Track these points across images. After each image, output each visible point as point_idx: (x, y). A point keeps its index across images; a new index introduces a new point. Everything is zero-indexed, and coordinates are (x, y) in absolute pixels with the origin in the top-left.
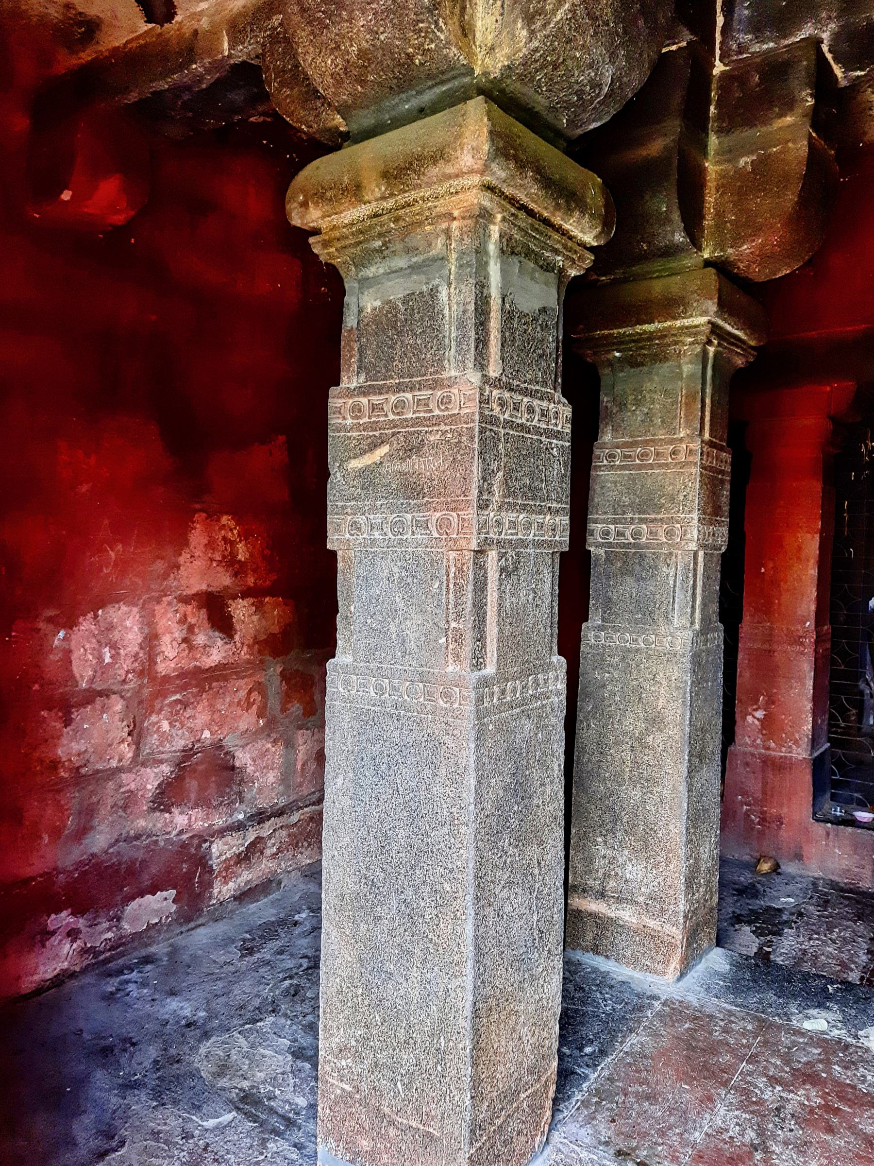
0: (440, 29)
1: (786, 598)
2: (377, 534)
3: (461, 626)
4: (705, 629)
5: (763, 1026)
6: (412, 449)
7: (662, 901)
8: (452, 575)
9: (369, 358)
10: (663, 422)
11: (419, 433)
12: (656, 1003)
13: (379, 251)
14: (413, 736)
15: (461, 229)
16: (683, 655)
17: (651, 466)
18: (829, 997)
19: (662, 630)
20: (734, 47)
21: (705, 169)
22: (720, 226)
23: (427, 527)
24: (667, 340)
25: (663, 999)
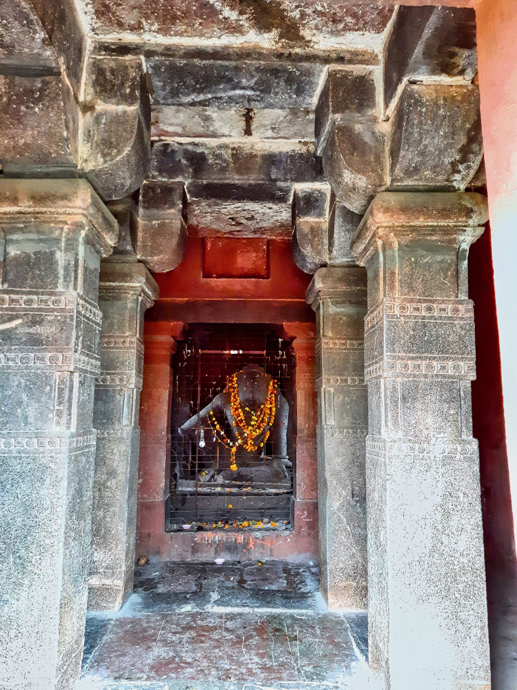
0: (68, 148)
1: (154, 420)
2: (11, 363)
3: (62, 408)
4: (135, 428)
5: (164, 616)
6: (34, 322)
7: (113, 568)
8: (57, 383)
9: (11, 276)
10: (118, 328)
11: (41, 315)
12: (112, 622)
13: (22, 228)
14: (30, 466)
15: (69, 229)
16: (128, 439)
17: (113, 348)
18: (188, 599)
19: (117, 427)
20: (151, 175)
21: (137, 221)
22: (144, 247)
23: (44, 360)
24: (122, 291)
25: (115, 619)
